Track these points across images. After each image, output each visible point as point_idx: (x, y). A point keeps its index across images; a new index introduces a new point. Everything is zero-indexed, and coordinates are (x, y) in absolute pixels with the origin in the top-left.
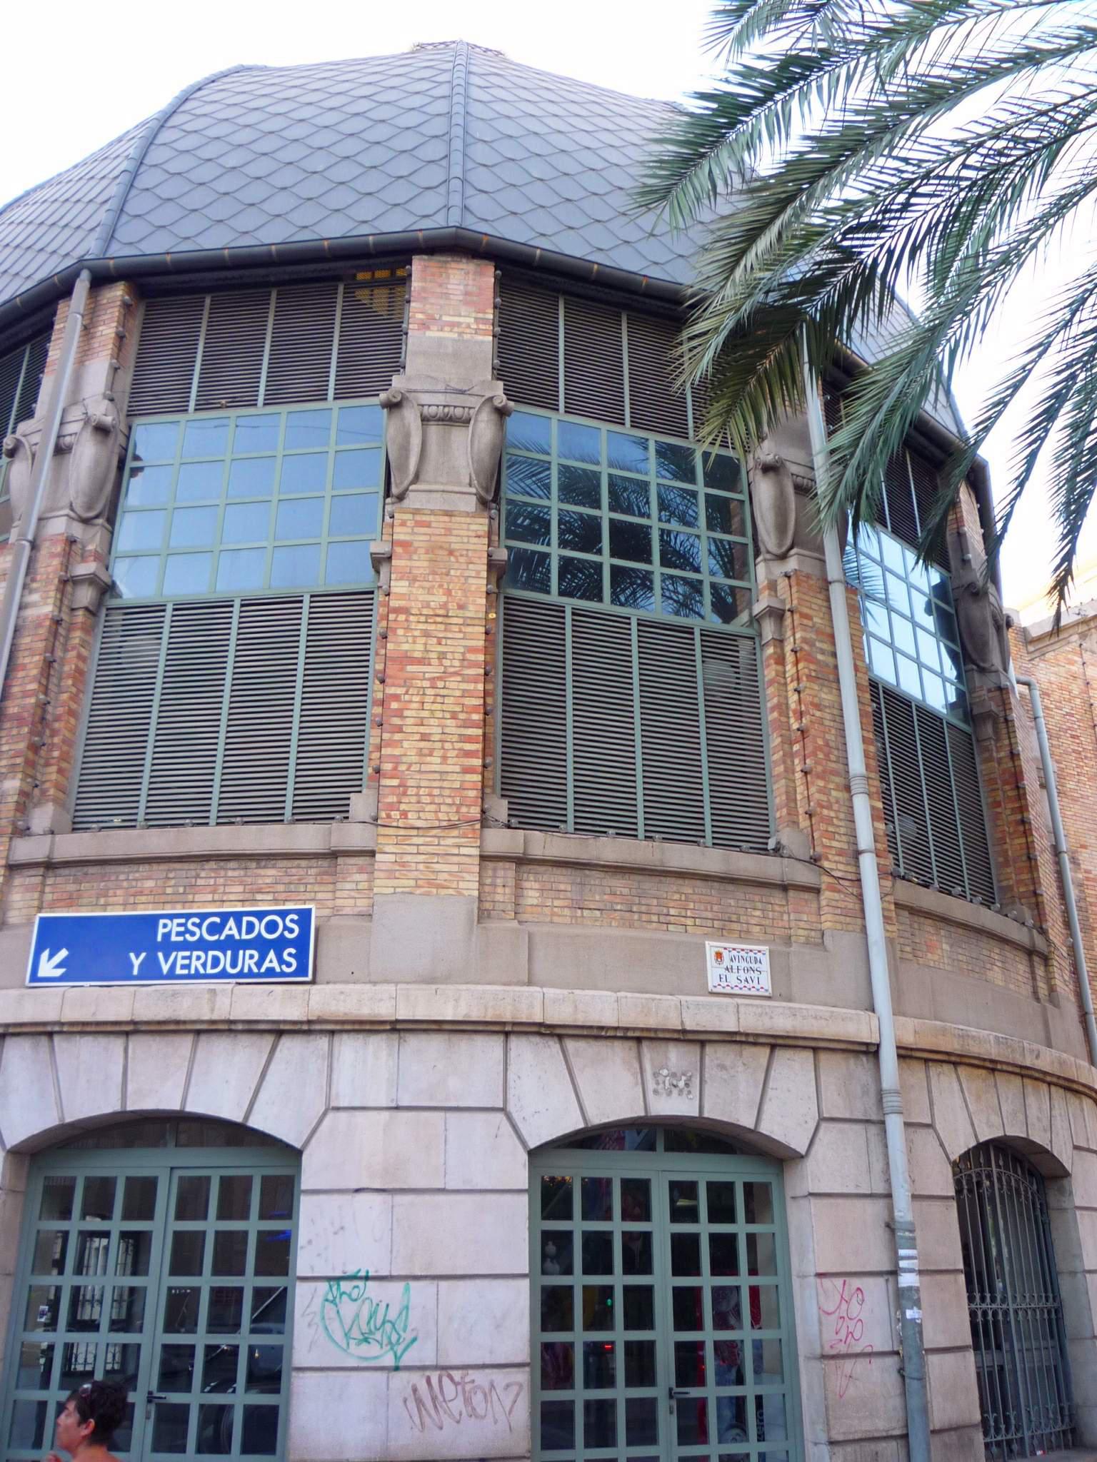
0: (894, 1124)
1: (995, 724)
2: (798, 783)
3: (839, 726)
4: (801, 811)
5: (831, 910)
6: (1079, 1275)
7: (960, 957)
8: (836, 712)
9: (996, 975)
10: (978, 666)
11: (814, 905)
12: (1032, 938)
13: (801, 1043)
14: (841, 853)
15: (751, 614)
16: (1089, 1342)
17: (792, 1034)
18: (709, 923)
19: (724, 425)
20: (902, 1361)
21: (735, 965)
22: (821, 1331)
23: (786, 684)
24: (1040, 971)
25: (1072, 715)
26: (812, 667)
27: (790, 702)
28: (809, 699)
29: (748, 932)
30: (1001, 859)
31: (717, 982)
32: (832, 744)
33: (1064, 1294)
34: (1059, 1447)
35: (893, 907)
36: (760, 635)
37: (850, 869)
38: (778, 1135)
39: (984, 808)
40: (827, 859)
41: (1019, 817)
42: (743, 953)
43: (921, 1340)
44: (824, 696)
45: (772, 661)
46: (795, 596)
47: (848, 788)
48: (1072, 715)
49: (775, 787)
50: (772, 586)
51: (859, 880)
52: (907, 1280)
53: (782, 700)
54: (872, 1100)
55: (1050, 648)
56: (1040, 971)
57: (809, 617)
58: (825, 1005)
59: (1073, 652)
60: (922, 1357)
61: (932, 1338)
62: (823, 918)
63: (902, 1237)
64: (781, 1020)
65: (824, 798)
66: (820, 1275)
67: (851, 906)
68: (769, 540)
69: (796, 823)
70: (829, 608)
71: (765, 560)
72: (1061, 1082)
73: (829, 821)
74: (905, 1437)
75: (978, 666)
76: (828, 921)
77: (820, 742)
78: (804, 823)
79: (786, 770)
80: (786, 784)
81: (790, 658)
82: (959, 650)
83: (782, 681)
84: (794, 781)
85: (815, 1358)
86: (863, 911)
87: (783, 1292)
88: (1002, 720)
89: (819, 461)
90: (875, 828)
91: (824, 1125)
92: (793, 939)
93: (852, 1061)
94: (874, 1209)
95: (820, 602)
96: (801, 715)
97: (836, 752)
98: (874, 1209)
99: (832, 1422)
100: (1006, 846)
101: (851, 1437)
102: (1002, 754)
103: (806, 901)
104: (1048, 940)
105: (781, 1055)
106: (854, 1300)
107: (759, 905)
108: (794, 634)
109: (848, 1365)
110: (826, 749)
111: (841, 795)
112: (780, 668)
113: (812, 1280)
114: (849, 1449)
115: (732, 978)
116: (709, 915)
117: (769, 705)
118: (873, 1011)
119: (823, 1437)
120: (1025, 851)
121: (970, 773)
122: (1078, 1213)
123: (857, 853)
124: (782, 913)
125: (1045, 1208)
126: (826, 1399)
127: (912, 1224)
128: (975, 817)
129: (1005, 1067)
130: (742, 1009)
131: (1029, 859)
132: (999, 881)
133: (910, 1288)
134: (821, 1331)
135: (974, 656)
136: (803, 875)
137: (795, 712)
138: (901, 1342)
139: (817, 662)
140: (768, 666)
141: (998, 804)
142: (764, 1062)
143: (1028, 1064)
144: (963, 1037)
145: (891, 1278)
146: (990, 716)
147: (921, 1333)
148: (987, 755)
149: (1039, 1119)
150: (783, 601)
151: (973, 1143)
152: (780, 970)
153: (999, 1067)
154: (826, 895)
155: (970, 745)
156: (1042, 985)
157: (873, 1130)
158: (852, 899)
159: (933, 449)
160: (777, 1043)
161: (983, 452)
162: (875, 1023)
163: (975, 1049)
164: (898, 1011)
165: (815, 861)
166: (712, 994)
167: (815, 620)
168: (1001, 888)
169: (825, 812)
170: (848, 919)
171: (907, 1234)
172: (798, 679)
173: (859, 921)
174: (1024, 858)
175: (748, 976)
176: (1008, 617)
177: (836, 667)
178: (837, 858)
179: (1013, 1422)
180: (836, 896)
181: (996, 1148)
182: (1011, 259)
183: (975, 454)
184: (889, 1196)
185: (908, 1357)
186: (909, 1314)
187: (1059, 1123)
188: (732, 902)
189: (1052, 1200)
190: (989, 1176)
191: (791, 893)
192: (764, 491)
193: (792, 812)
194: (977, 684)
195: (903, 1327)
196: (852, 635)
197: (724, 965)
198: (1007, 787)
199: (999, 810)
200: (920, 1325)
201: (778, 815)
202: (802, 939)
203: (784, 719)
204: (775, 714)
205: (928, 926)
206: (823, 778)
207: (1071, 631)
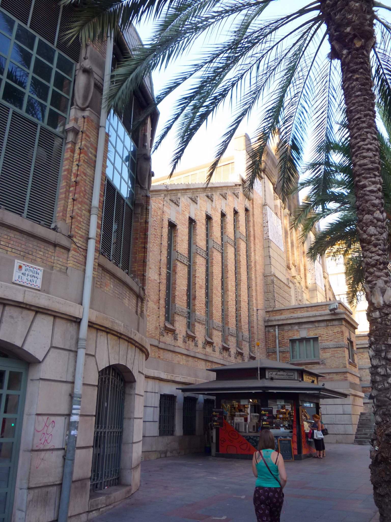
0: (81, 353)
1: (142, 209)
2: (69, 204)
3: (92, 185)
4: (68, 215)
5: (73, 259)
6: (132, 419)
7: (116, 292)
8: (91, 179)
9: (126, 301)
10: (140, 186)
11: (66, 256)
12: (140, 291)
13: (49, 312)
14: (81, 237)
15: (64, 129)
16: (131, 445)
17: (46, 308)
18: (18, 252)
19: (79, 31)
20: (66, 452)
21: (27, 273)
22: (33, 439)
23: (73, 162)
24: (140, 304)
25: (156, 222)
26: (86, 157)
27: (73, 169)
28: (82, 170)
29: (35, 260)
30: (133, 260)
31: (17, 278)
32: (87, 191)
33: (124, 426)
34: (113, 485)
35: (97, 264)
36: (66, 139)
37: (83, 244)
38: (31, 351)
39: (132, 239)
40: (75, 238)
41: (143, 245)
42: (31, 269)
43: (76, 444)
44: (88, 171)
45: (69, 150)
46: (85, 126)
47: (90, 211)
48: (156, 222)
49: (59, 203)
50: (76, 120)
51: (87, 250)
52: (74, 418)
53: (70, 168)
54: (74, 342)
55: (154, 196)
56: (140, 304)
57: (89, 138)
58: (63, 298)
59: (161, 200)
60: (74, 451)
61: (80, 443)
62: (69, 262)
63: (75, 400)
64: (43, 301)
65: (79, 212)
66: (38, 415)
67: (81, 260)
68: (79, 100)
69: (65, 220)
70: (98, 137)
71: (75, 108)
72: (140, 346)
73: (80, 222)
74: (61, 484)
75: (140, 186)
76: (70, 264)
77: (83, 189)
78: (68, 220)
79: (65, 197)
80: (63, 204)
81: (77, 151)
82: (135, 177)
83: (72, 160)
84: (68, 202)
85: (28, 451)
86: (85, 263)
87: (19, 422)
88: (145, 208)
89: (107, 78)
90: (97, 231)
91: (52, 350)
92: (54, 268)
93: (69, 324)
94: (66, 388)
95: (95, 133)
96: (77, 176)
97: (88, 195)
98: (66, 388)
99: (31, 479)
100: (136, 255)
101: (38, 486)
102: (142, 221)
103: (63, 253)
104: (144, 293)
105: (40, 317)
106: (51, 426)
107: (43, 250)
108: (81, 142)
109: (43, 454)
110: (84, 193)
111: (87, 214)
112: (72, 154)
113: (34, 416)
114: (36, 491)
115: (24, 278)
116: (20, 249)
117: (64, 168)
118: (82, 305)
119: (26, 486)
120: (143, 259)
121: (129, 225)
122: (136, 396)
123: (88, 239)
124: (51, 256)
125: (124, 393)
126: (30, 469)
127: (81, 395)
128: (128, 241)
129: (124, 337)
130: (26, 293)
131: (144, 262)
132: (131, 268)
133: (75, 422)
134: (33, 439)
135: (140, 181)
136: (65, 242)
137: (74, 174)
138: (66, 445)
139: (89, 157)
140: (67, 152)
141: (137, 239)
142: (31, 318)
143: (132, 337)
144: (113, 322)
145: (67, 417)
146: (141, 205)
147: (76, 441)
148: (137, 220)
149: (130, 359)
150: (80, 127)
151: (108, 365)
152: (46, 279)
153: (122, 337)
154: (72, 253)
155: (131, 214)
156: (139, 309)
157: (72, 354)
158: (83, 257)
159: (143, 99)
160: (39, 311)
161: (160, 107)
162: (82, 310)
163: (116, 328)
164: (91, 307)
165: (70, 237)
166: (14, 283)
167: (91, 139)
168: (131, 270)
169: (79, 218)
170: (79, 265)
171: (78, 399)
172: (79, 161)
173: (83, 267)
174: (142, 261)
175: (32, 279)
176: (153, 173)
177: (95, 161)
178: (79, 238)
179: (100, 476)
180: (76, 254)
181: (113, 369)
182: (196, 29)
183: (156, 106)
184: (73, 383)
185: (68, 451)
186: (73, 432)
187: (136, 362)
188: (31, 246)
189: (127, 391)
190: (109, 379)
191: (57, 248)
192: (82, 80)
193: (64, 215)
194: (139, 192)
195: (68, 438)
196: (104, 151)
197: (22, 272)
198: (141, 234)
199: (137, 241)
200: (76, 437)
201: (58, 215)
202: (58, 269)
203: (69, 175)
204: (66, 173)
205: (108, 276)
206: (81, 204)
207: (162, 192)
